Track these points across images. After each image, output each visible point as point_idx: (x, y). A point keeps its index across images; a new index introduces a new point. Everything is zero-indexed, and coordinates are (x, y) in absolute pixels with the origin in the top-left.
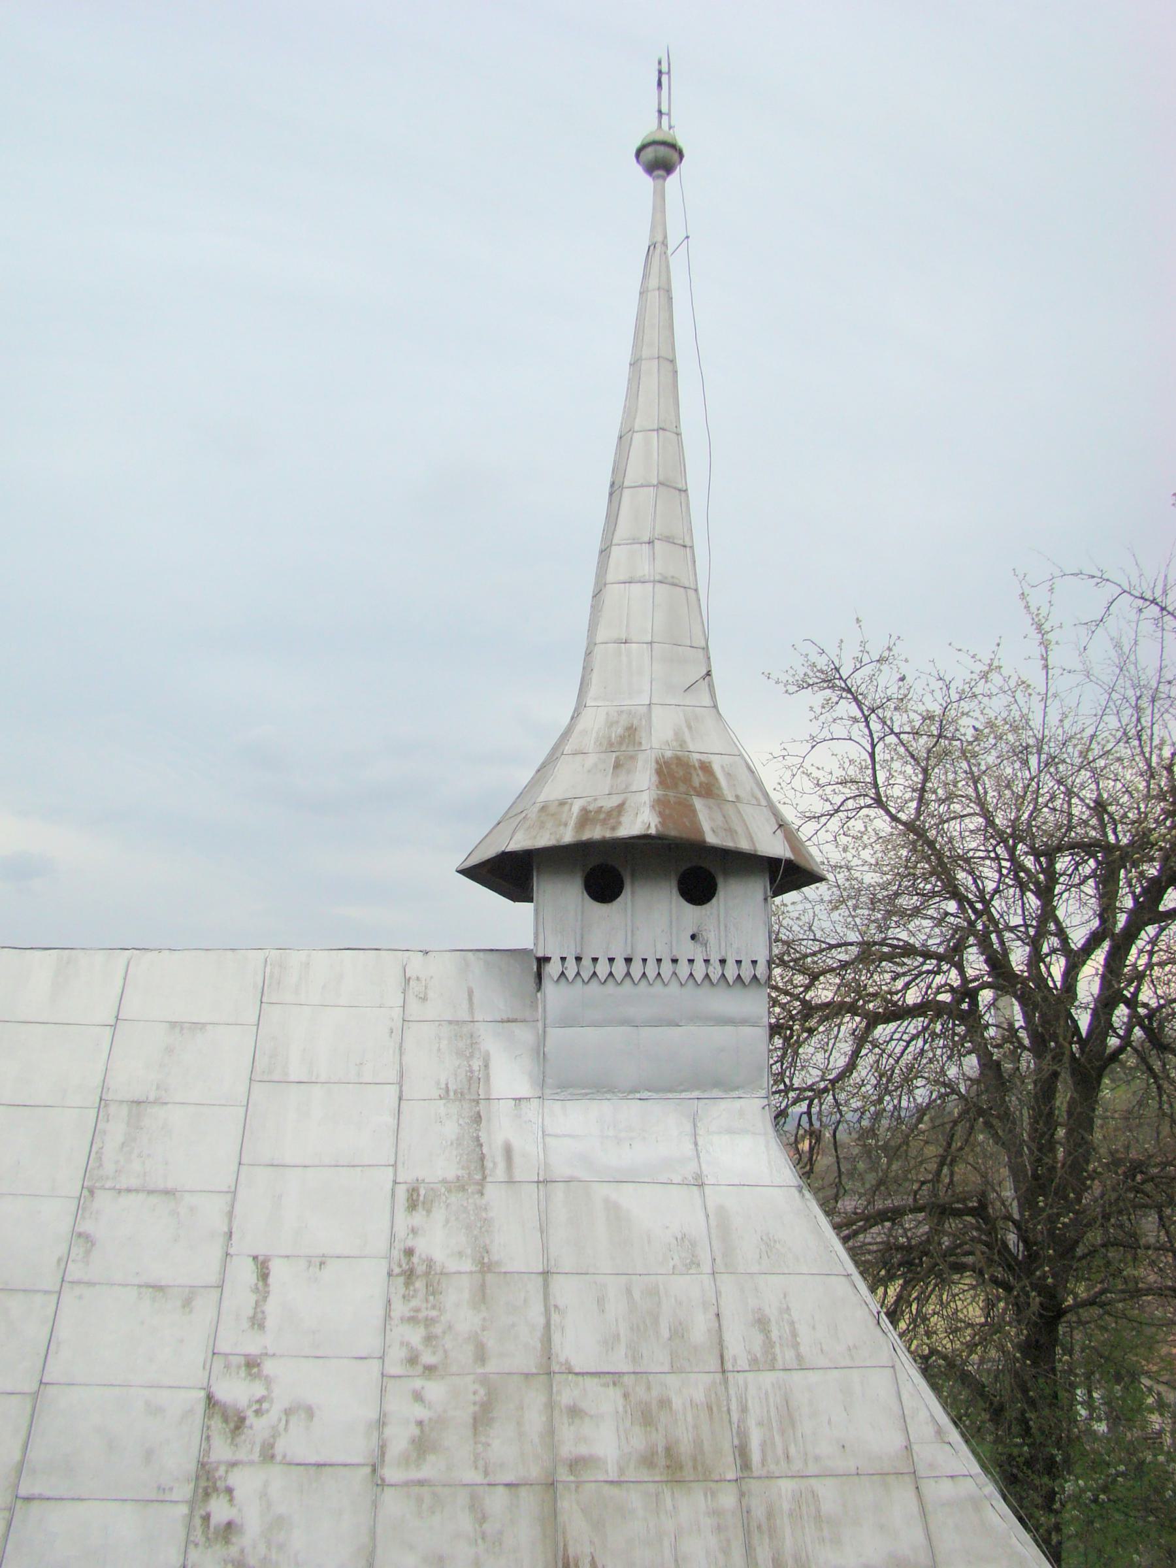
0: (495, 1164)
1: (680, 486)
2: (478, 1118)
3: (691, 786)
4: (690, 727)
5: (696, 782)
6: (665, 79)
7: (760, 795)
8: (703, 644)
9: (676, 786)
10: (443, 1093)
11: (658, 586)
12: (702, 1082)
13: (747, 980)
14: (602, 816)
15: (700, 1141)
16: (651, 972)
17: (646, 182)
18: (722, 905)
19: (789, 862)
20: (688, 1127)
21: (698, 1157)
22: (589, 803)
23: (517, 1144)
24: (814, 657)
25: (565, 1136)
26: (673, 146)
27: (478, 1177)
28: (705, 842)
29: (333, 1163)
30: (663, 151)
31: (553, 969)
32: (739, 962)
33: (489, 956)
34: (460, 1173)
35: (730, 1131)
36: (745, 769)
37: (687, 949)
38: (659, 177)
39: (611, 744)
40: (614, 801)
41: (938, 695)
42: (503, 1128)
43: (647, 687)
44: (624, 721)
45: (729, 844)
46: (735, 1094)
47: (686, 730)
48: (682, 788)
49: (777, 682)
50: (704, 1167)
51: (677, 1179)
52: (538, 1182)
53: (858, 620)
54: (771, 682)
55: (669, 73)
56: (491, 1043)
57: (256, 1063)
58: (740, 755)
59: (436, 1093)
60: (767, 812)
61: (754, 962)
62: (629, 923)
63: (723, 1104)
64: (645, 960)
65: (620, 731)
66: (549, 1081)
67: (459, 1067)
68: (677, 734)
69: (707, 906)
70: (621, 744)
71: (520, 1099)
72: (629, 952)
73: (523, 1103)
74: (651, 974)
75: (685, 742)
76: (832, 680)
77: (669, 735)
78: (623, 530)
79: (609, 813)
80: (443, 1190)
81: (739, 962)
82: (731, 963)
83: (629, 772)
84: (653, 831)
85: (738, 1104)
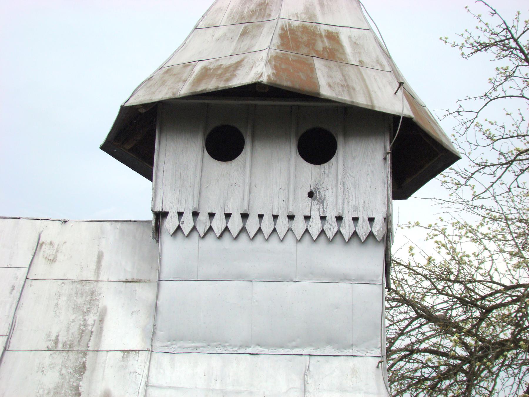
2: (82, 369)
5: (320, 46)
7: (385, 62)
10: (51, 344)
13: (363, 237)
14: (220, 72)
18: (340, 167)
19: (408, 120)
20: (298, 383)
28: (319, 94)
31: (170, 224)
32: (355, 220)
33: (126, 226)
36: (374, 41)
37: (303, 206)
39: (242, 17)
45: (345, 97)
46: (350, 352)
47: (318, 8)
49: (453, 46)
54: (448, 45)
56: (111, 299)
60: (390, 77)
61: (371, 220)
62: (247, 180)
64: (261, 216)
66: (159, 333)
67: (73, 321)
68: (308, 10)
69: (326, 165)
70: (251, 16)
71: (129, 351)
72: (246, 207)
73: (132, 355)
74: (267, 229)
75: (315, 16)
77: (300, 8)
79: (227, 69)
83: (253, 37)
84: (264, 80)
85: (352, 362)
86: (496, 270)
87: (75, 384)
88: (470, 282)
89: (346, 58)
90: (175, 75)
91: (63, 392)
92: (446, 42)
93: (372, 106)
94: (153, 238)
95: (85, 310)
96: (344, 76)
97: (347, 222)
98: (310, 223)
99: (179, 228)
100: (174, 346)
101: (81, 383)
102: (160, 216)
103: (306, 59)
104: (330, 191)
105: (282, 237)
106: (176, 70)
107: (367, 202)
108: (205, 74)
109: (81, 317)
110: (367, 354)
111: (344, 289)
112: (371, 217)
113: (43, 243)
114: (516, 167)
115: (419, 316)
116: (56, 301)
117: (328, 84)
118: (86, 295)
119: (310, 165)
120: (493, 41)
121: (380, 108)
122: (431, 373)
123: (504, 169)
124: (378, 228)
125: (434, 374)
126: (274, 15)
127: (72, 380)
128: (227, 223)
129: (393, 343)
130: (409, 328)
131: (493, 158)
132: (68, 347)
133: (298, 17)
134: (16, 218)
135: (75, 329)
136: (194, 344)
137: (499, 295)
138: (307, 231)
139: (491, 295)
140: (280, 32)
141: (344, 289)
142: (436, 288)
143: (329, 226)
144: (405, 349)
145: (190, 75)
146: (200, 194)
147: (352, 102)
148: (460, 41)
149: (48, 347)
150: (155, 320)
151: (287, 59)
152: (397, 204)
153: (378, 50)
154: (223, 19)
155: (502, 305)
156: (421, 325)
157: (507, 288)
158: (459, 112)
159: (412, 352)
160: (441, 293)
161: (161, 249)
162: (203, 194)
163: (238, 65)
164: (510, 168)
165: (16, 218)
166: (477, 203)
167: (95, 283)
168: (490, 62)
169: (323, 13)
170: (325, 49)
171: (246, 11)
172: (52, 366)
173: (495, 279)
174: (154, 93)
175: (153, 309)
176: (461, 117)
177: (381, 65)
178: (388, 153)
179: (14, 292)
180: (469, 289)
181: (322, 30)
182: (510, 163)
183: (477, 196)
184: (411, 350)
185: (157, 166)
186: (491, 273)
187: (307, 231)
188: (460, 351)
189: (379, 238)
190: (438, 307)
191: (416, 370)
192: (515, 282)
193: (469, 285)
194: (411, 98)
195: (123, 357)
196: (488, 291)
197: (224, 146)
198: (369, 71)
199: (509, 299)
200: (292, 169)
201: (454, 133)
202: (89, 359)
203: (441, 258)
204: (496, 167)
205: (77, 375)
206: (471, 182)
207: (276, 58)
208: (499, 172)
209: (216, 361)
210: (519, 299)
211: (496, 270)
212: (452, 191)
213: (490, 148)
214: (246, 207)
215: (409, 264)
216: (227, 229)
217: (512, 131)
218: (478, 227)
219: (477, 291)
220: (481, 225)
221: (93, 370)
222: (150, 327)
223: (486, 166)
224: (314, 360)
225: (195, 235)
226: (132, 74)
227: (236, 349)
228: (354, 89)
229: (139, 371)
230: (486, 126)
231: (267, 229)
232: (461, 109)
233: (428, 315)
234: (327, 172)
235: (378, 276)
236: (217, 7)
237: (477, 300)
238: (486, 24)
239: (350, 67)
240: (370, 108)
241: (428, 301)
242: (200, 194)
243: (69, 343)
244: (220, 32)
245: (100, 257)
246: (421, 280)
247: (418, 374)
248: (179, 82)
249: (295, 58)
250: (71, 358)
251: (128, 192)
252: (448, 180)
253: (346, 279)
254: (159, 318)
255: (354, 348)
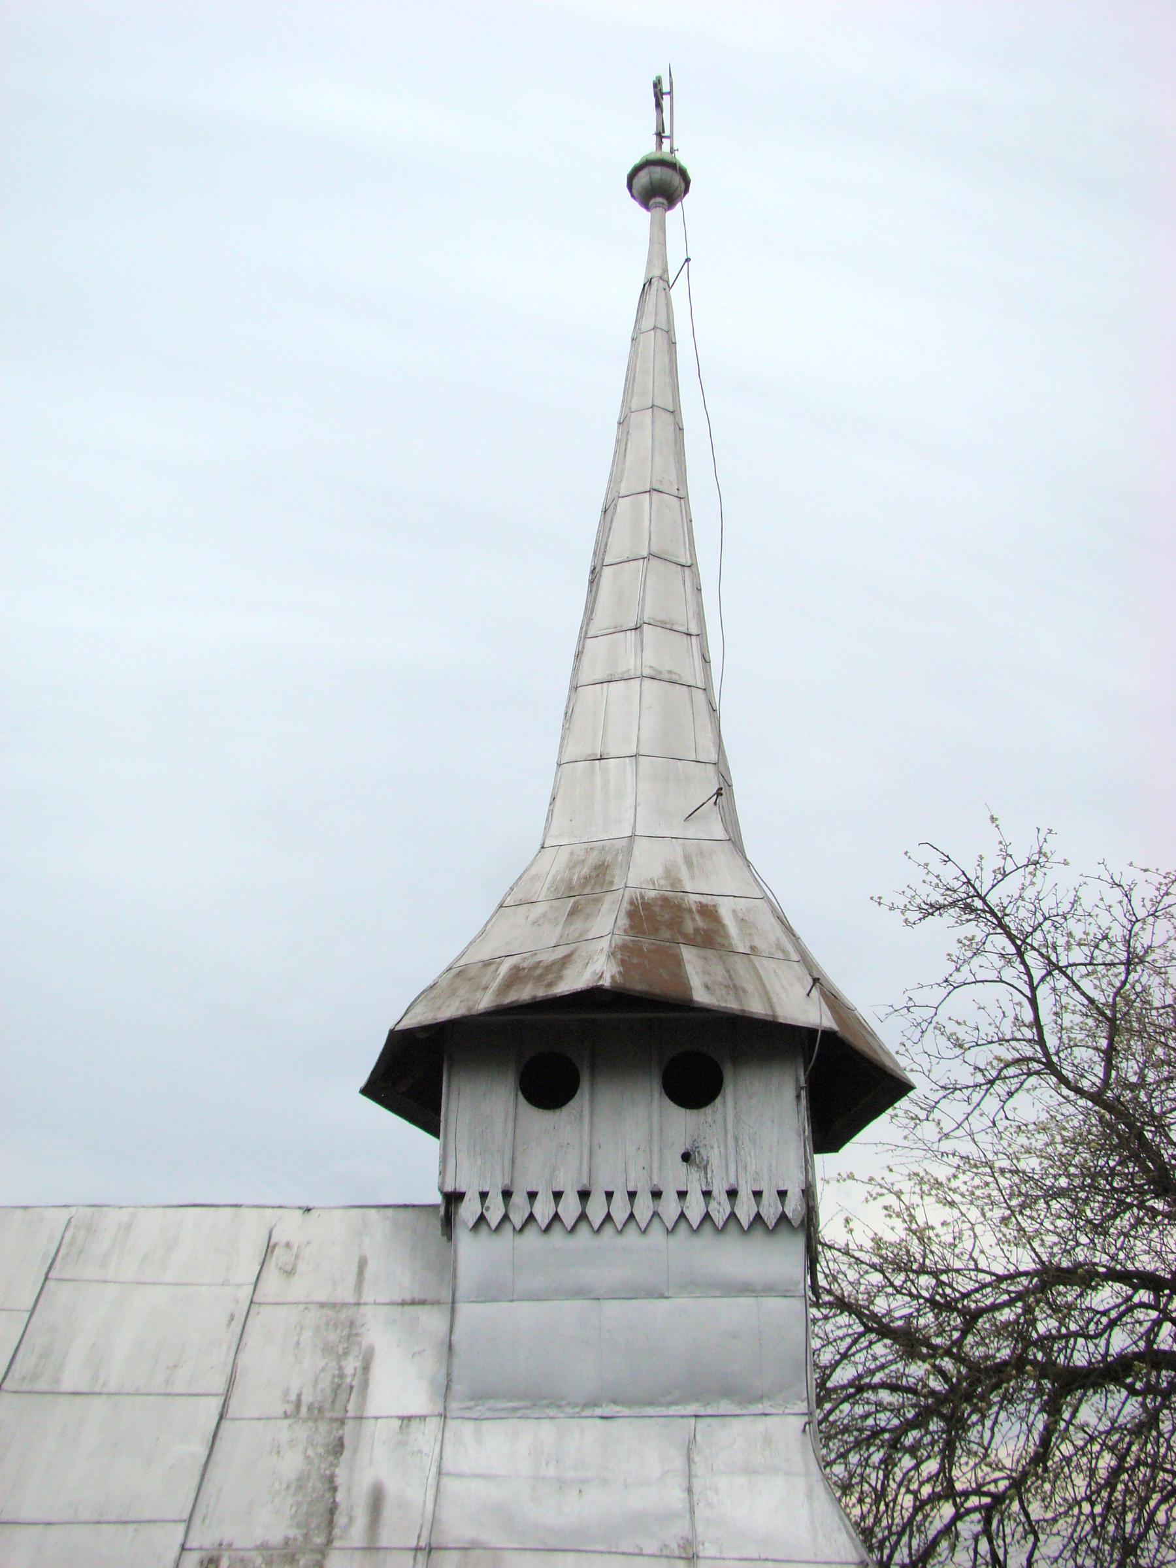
0: (351, 1519)
1: (683, 561)
2: (338, 1448)
3: (679, 932)
4: (689, 862)
6: (666, 101)
7: (789, 947)
8: (714, 757)
9: (656, 930)
10: (290, 1408)
11: (647, 683)
12: (705, 1390)
13: (771, 1223)
14: (538, 972)
15: (697, 1485)
16: (620, 1212)
17: (640, 217)
18: (730, 1111)
19: (828, 1034)
20: (679, 1463)
21: (692, 1511)
22: (524, 959)
23: (392, 1487)
24: (937, 867)
25: (476, 1476)
26: (673, 166)
27: (319, 1540)
28: (691, 1000)
29: (95, 1517)
30: (658, 172)
31: (468, 1211)
33: (401, 1214)
34: (292, 1533)
35: (750, 1470)
37: (676, 1175)
38: (659, 210)
39: (570, 887)
40: (561, 952)
41: (1118, 911)
42: (375, 1462)
43: (629, 815)
44: (593, 859)
45: (731, 1004)
46: (759, 1408)
48: (666, 934)
50: (700, 1528)
51: (651, 1547)
52: (417, 1549)
53: (993, 819)
55: (670, 93)
56: (381, 1335)
57: (15, 1366)
58: (765, 898)
59: (278, 1409)
60: (799, 969)
61: (782, 1194)
62: (586, 1138)
63: (737, 1427)
64: (609, 1195)
65: (585, 870)
66: (456, 1387)
67: (323, 1369)
69: (708, 1110)
70: (584, 886)
71: (409, 1418)
72: (585, 1181)
73: (414, 1424)
74: (620, 1216)
75: (680, 881)
76: (970, 903)
77: (657, 871)
78: (601, 621)
79: (548, 968)
80: (259, 1560)
81: (758, 1194)
82: (745, 1195)
83: (588, 917)
84: (606, 982)
85: (762, 1425)
86: (982, 1252)
87: (328, 1472)
88: (946, 1272)
89: (731, 945)
90: (470, 979)
91: (310, 1485)
92: (880, 904)
93: (774, 1016)
94: (443, 1234)
95: (340, 1352)
96: (728, 971)
97: (745, 1199)
98: (687, 1203)
99: (482, 1218)
100: (480, 1408)
101: (337, 1471)
102: (453, 1198)
103: (668, 947)
104: (716, 1149)
105: (643, 1226)
106: (472, 972)
107: (774, 1165)
108: (516, 977)
109: (334, 1364)
110: (787, 1411)
111: (748, 1304)
112: (782, 1188)
113: (274, 1247)
114: (1000, 1088)
115: (868, 1330)
116: (296, 1339)
117: (703, 983)
118: (342, 1328)
119: (682, 1111)
120: (950, 900)
121: (785, 1018)
122: (889, 1420)
123: (982, 1092)
124: (794, 1206)
125: (895, 1422)
126: (618, 883)
127: (323, 1466)
128: (557, 1205)
129: (829, 1376)
130: (854, 1349)
131: (965, 1076)
132: (316, 1412)
133: (654, 883)
134: (236, 1206)
135: (325, 1383)
136: (512, 1404)
137: (989, 1290)
138: (682, 1215)
139: (976, 1290)
140: (629, 907)
141: (748, 1304)
142: (892, 1285)
143: (716, 1205)
144: (851, 1384)
145: (494, 979)
146: (513, 1162)
147: (743, 1011)
148: (901, 901)
149: (285, 1413)
150: (449, 1366)
151: (641, 949)
152: (823, 1161)
153: (779, 929)
154: (541, 890)
155: (995, 1307)
156: (871, 1343)
157: (1000, 1279)
158: (908, 1009)
159: (860, 1389)
160: (899, 1292)
161: (455, 1248)
162: (518, 1161)
163: (565, 961)
164: (992, 1090)
165: (236, 1206)
166: (946, 1145)
167: (355, 1308)
168: (947, 931)
169: (692, 877)
170: (697, 930)
171: (575, 878)
172: (292, 1442)
173: (982, 1264)
174: (439, 1008)
175: (446, 1346)
176: (913, 1016)
177: (783, 951)
178: (802, 1088)
179: (234, 1323)
180: (943, 1283)
181: (692, 903)
182: (991, 1082)
183: (947, 1136)
184: (859, 1387)
185: (446, 1120)
186: (975, 1255)
187: (682, 1215)
188: (936, 1384)
189: (796, 1223)
190: (897, 1314)
191: (865, 1417)
192: (1012, 1268)
193: (944, 1278)
194: (833, 1000)
195: (401, 1427)
196: (971, 1286)
197: (548, 1087)
198: (765, 962)
199: (1005, 1297)
200: (655, 1117)
201: (904, 1040)
202: (348, 1431)
203: (894, 1232)
204: (970, 1090)
205: (331, 1458)
206: (936, 1114)
207: (624, 948)
208: (976, 1097)
209: (546, 1431)
210: (1020, 1296)
211: (982, 1252)
212: (906, 1132)
213: (959, 1061)
214: (585, 1181)
215: (847, 1245)
216: (556, 1217)
217: (991, 1033)
218: (949, 1180)
219: (955, 1285)
220: (955, 1176)
221: (355, 1450)
222: (442, 1377)
223: (956, 1089)
224: (702, 1424)
225: (508, 1228)
226: (400, 981)
227: (578, 1410)
228: (744, 991)
229: (426, 1449)
230: (951, 1027)
231: (620, 1216)
232: (911, 1004)
233: (880, 1328)
234: (709, 1120)
235: (797, 1284)
236: (533, 872)
237: (956, 1300)
238: (938, 877)
239: (737, 958)
240: (771, 1019)
241: (880, 1305)
242: (513, 1162)
243: (316, 1405)
244: (537, 911)
245: (362, 1264)
246: (867, 1272)
247: (870, 1421)
248: (477, 989)
249: (653, 947)
250: (321, 1429)
251: (405, 1159)
252: (900, 1113)
253: (745, 1289)
254: (456, 1362)
255: (765, 1400)
